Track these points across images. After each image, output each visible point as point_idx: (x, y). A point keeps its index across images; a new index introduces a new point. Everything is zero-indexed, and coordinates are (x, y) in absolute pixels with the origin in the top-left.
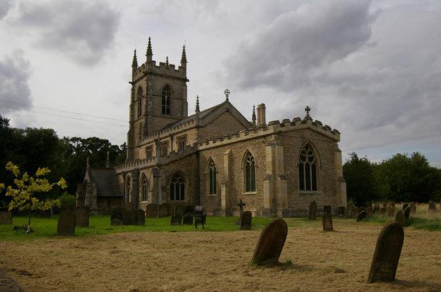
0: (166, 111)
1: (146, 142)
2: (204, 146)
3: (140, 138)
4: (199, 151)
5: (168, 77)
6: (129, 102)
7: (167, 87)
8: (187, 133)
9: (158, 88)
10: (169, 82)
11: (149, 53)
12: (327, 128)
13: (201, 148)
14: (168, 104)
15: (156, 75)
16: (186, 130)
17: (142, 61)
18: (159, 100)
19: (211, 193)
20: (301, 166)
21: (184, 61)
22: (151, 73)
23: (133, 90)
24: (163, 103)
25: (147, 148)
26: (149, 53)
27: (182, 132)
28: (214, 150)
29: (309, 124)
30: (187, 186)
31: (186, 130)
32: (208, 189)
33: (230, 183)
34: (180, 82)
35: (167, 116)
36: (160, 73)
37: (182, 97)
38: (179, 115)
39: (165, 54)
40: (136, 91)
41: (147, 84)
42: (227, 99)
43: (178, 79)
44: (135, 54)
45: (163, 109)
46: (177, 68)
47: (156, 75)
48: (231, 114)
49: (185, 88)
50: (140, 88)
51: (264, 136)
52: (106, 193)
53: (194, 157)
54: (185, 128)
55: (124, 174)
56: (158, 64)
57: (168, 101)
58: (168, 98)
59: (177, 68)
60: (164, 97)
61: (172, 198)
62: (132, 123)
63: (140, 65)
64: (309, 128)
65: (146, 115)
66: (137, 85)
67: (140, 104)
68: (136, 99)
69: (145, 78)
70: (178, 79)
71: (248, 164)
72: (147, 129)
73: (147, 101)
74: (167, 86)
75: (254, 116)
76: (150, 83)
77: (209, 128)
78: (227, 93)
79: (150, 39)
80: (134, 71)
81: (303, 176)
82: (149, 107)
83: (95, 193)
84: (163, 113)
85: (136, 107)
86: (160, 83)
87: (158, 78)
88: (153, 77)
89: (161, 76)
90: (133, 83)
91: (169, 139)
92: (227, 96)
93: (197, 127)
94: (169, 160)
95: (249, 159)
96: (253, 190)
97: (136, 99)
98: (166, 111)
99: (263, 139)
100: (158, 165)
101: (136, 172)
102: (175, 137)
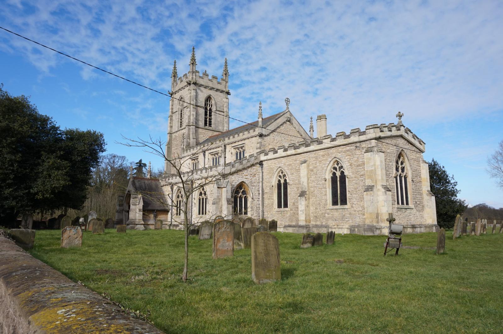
4: (262, 161)
7: (209, 98)
10: (212, 93)
64: (401, 136)
86: (203, 95)
89: (206, 87)
96: (346, 204)
102: (207, 153)
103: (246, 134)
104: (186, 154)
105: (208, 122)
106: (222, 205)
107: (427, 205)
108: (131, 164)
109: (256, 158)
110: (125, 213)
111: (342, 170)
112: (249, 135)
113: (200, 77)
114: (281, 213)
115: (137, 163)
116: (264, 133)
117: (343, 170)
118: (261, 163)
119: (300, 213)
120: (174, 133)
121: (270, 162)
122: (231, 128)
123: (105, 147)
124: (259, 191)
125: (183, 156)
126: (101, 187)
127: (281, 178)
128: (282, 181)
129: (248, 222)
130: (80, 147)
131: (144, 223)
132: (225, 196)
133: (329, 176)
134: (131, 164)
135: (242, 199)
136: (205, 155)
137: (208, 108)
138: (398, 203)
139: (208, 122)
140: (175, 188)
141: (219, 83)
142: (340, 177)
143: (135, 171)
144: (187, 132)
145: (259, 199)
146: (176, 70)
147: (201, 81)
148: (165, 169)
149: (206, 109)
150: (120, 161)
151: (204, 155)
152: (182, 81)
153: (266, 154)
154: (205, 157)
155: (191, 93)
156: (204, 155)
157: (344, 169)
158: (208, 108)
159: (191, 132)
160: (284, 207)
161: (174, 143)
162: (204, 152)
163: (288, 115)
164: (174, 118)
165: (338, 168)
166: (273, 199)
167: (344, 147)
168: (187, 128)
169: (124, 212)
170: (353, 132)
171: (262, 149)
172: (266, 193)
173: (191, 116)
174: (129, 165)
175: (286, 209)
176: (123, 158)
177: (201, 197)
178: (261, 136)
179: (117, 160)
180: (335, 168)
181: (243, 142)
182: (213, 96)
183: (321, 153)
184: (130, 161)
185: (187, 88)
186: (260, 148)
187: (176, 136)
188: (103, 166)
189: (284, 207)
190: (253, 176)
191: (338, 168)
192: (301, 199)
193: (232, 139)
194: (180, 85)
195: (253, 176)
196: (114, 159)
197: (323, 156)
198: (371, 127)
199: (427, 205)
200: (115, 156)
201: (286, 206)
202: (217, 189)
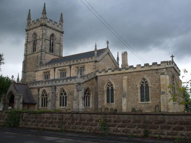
0: (52, 50)
1: (44, 68)
4: (97, 76)
5: (54, 29)
7: (52, 35)
8: (85, 64)
10: (54, 32)
12: (178, 68)
14: (53, 46)
15: (47, 27)
16: (85, 63)
20: (61, 97)
24: (50, 45)
28: (112, 76)
29: (173, 65)
30: (91, 98)
31: (85, 63)
34: (59, 33)
35: (52, 53)
36: (50, 26)
42: (108, 46)
45: (50, 49)
48: (110, 56)
49: (62, 37)
50: (35, 34)
51: (157, 70)
52: (27, 101)
53: (94, 80)
57: (53, 44)
58: (52, 42)
60: (50, 41)
62: (26, 55)
63: (33, 18)
66: (32, 32)
71: (108, 88)
73: (42, 43)
75: (118, 58)
76: (44, 32)
77: (100, 62)
80: (29, 24)
81: (111, 98)
82: (43, 47)
83: (21, 101)
84: (50, 51)
85: (30, 46)
86: (49, 32)
87: (48, 29)
89: (50, 28)
90: (27, 30)
92: (172, 58)
94: (84, 81)
98: (52, 50)
99: (156, 71)
101: (53, 87)
102: (56, 69)
103: (86, 60)
105: (51, 50)
106: (79, 101)
109: (95, 74)
112: (88, 61)
113: (48, 22)
118: (96, 78)
119: (123, 105)
120: (29, 55)
121: (102, 77)
122: (64, 55)
125: (37, 70)
128: (144, 85)
130: (180, 82)
132: (81, 96)
133: (139, 86)
136: (55, 70)
138: (85, 106)
139: (51, 50)
140: (41, 90)
141: (58, 26)
144: (40, 55)
146: (30, 15)
147: (48, 24)
148: (20, 78)
151: (55, 71)
153: (100, 72)
154: (55, 72)
155: (43, 31)
156: (55, 71)
158: (52, 41)
160: (111, 102)
161: (29, 61)
162: (55, 68)
163: (108, 51)
164: (28, 45)
165: (144, 82)
167: (148, 71)
168: (40, 53)
169: (6, 104)
171: (96, 70)
173: (43, 46)
175: (112, 104)
178: (96, 62)
180: (142, 82)
183: (135, 74)
185: (40, 28)
186: (95, 69)
187: (30, 57)
189: (111, 102)
191: (144, 82)
193: (75, 62)
197: (136, 75)
201: (112, 101)
202: (76, 91)
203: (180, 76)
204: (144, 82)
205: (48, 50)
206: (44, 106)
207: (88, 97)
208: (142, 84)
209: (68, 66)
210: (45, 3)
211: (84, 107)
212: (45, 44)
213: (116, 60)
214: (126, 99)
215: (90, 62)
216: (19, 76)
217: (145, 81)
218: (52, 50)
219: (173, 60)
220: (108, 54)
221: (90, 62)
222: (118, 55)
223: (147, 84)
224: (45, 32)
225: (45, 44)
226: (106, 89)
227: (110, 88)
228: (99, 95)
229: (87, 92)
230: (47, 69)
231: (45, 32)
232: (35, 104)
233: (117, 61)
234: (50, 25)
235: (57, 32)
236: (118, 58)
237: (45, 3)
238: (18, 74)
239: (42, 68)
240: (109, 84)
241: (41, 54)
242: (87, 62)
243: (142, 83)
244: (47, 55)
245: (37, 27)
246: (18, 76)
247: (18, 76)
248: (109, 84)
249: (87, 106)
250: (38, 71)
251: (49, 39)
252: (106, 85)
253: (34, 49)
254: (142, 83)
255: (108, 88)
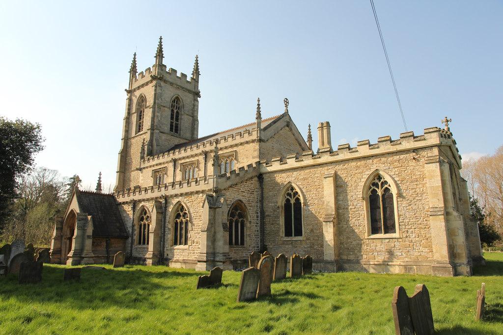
0: (175, 128)
2: (276, 166)
3: (142, 158)
5: (179, 87)
6: (123, 113)
7: (177, 100)
9: (167, 111)
10: (180, 93)
11: (160, 54)
13: (269, 169)
14: (177, 120)
16: (236, 145)
17: (147, 62)
18: (168, 112)
19: (288, 233)
21: (196, 71)
22: (161, 79)
23: (130, 100)
24: (172, 118)
25: (155, 172)
26: (160, 54)
27: (192, 156)
29: (450, 142)
31: (236, 145)
32: (283, 229)
33: (340, 218)
36: (170, 80)
37: (193, 114)
38: (188, 135)
39: (179, 62)
40: (135, 100)
41: (155, 90)
43: (189, 91)
44: (135, 58)
45: (171, 126)
46: (189, 79)
47: (165, 81)
48: (291, 130)
50: (142, 99)
51: (415, 150)
54: (193, 153)
55: (135, 203)
56: (179, 75)
58: (177, 112)
59: (189, 79)
61: (231, 243)
63: (140, 69)
65: (152, 128)
66: (137, 93)
67: (140, 117)
68: (134, 110)
69: (151, 85)
70: (189, 91)
71: (374, 192)
72: (152, 146)
73: (154, 112)
74: (177, 98)
75: (310, 137)
78: (286, 102)
79: (135, 55)
84: (171, 129)
85: (134, 118)
86: (169, 93)
87: (168, 86)
88: (162, 84)
89: (172, 84)
90: (129, 92)
91: (201, 159)
92: (286, 106)
93: (260, 140)
94: (229, 183)
95: (289, 195)
96: (389, 228)
97: (134, 110)
98: (175, 128)
99: (413, 155)
100: (217, 190)
104: (147, 164)
106: (215, 232)
107: (471, 233)
108: (64, 178)
110: (65, 240)
111: (386, 186)
114: (292, 243)
115: (71, 178)
116: (263, 138)
117: (389, 187)
123: (42, 144)
124: (258, 213)
126: (28, 206)
127: (291, 198)
129: (282, 260)
131: (93, 256)
134: (64, 178)
135: (238, 224)
137: (175, 111)
142: (383, 196)
143: (68, 187)
145: (258, 224)
149: (172, 111)
150: (51, 174)
152: (143, 76)
157: (390, 186)
158: (175, 111)
159: (154, 138)
166: (279, 224)
170: (362, 144)
172: (268, 216)
173: (155, 118)
174: (61, 180)
176: (55, 172)
177: (178, 221)
179: (47, 173)
181: (235, 149)
182: (181, 97)
184: (64, 175)
188: (30, 180)
189: (295, 235)
190: (250, 193)
192: (327, 225)
194: (141, 81)
195: (250, 193)
196: (44, 172)
198: (431, 130)
199: (471, 233)
200: (45, 170)
203: (460, 171)
204: (377, 179)
205: (167, 128)
206: (144, 243)
207: (234, 224)
208: (288, 197)
209: (200, 154)
210: (161, 37)
211: (227, 247)
212: (159, 114)
213: (306, 139)
214: (334, 226)
215: (247, 142)
216: (101, 180)
217: (382, 180)
218: (177, 127)
219: (449, 129)
220: (288, 126)
221: (247, 142)
222: (310, 129)
223: (298, 200)
224: (160, 91)
225: (159, 114)
226: (283, 204)
227: (293, 201)
228: (268, 217)
229: (237, 210)
230: (160, 164)
231: (160, 91)
232: (127, 238)
233: (308, 144)
234: (171, 78)
235: (187, 94)
236: (310, 137)
237: (161, 37)
238: (100, 174)
239: (152, 163)
240: (290, 191)
241: (152, 135)
242: (241, 144)
243: (287, 197)
244: (164, 137)
245: (147, 84)
246: (100, 178)
247: (100, 178)
248: (290, 191)
249: (237, 243)
250: (144, 168)
251: (169, 104)
252: (283, 193)
253: (139, 128)
254: (287, 197)
255: (288, 201)
